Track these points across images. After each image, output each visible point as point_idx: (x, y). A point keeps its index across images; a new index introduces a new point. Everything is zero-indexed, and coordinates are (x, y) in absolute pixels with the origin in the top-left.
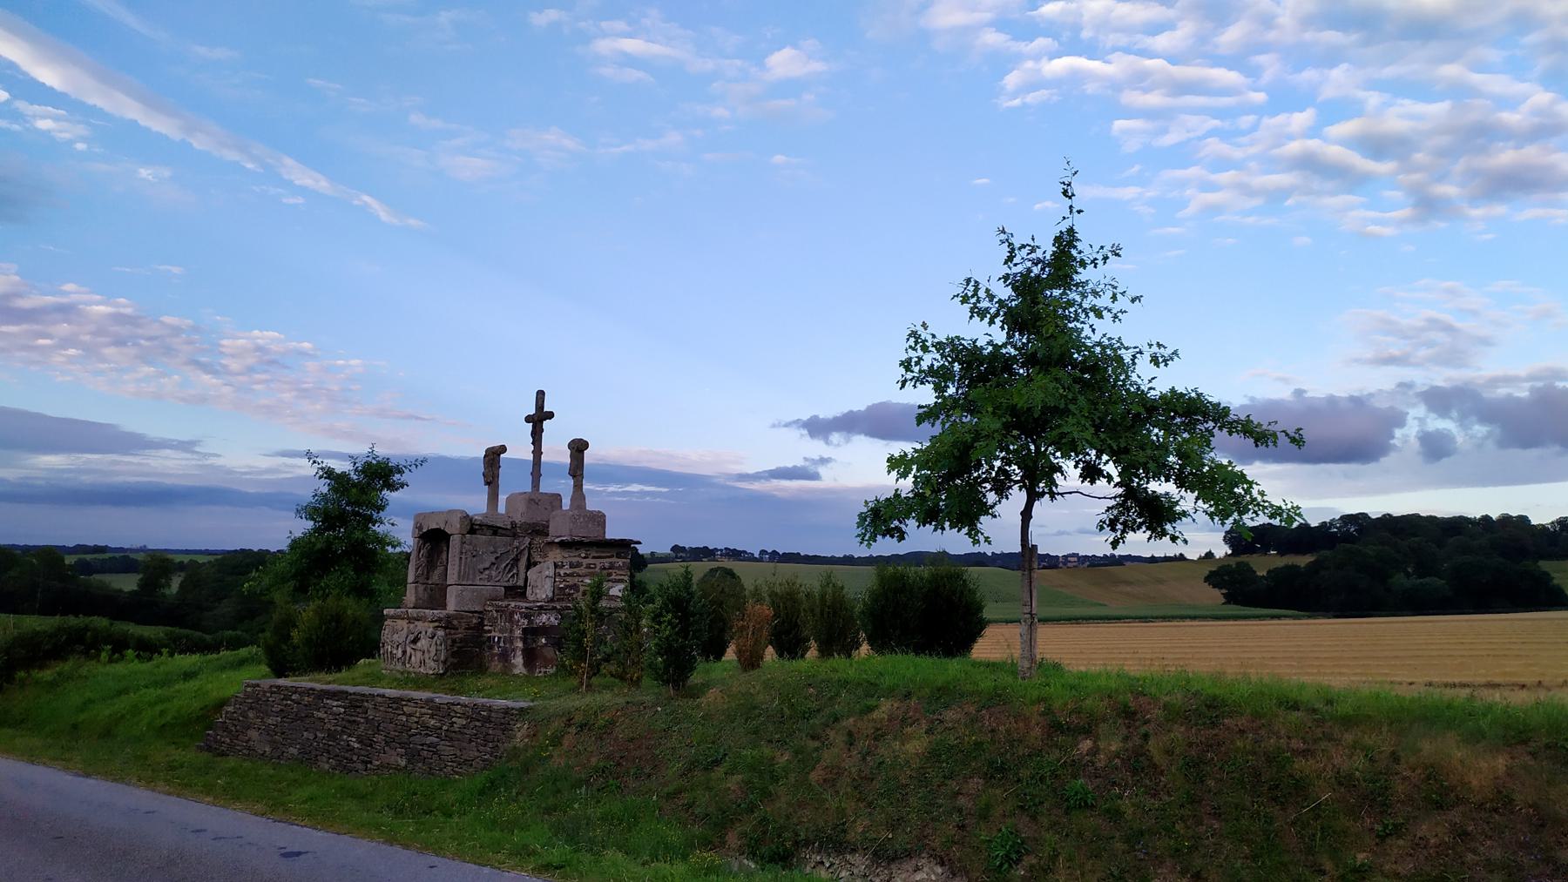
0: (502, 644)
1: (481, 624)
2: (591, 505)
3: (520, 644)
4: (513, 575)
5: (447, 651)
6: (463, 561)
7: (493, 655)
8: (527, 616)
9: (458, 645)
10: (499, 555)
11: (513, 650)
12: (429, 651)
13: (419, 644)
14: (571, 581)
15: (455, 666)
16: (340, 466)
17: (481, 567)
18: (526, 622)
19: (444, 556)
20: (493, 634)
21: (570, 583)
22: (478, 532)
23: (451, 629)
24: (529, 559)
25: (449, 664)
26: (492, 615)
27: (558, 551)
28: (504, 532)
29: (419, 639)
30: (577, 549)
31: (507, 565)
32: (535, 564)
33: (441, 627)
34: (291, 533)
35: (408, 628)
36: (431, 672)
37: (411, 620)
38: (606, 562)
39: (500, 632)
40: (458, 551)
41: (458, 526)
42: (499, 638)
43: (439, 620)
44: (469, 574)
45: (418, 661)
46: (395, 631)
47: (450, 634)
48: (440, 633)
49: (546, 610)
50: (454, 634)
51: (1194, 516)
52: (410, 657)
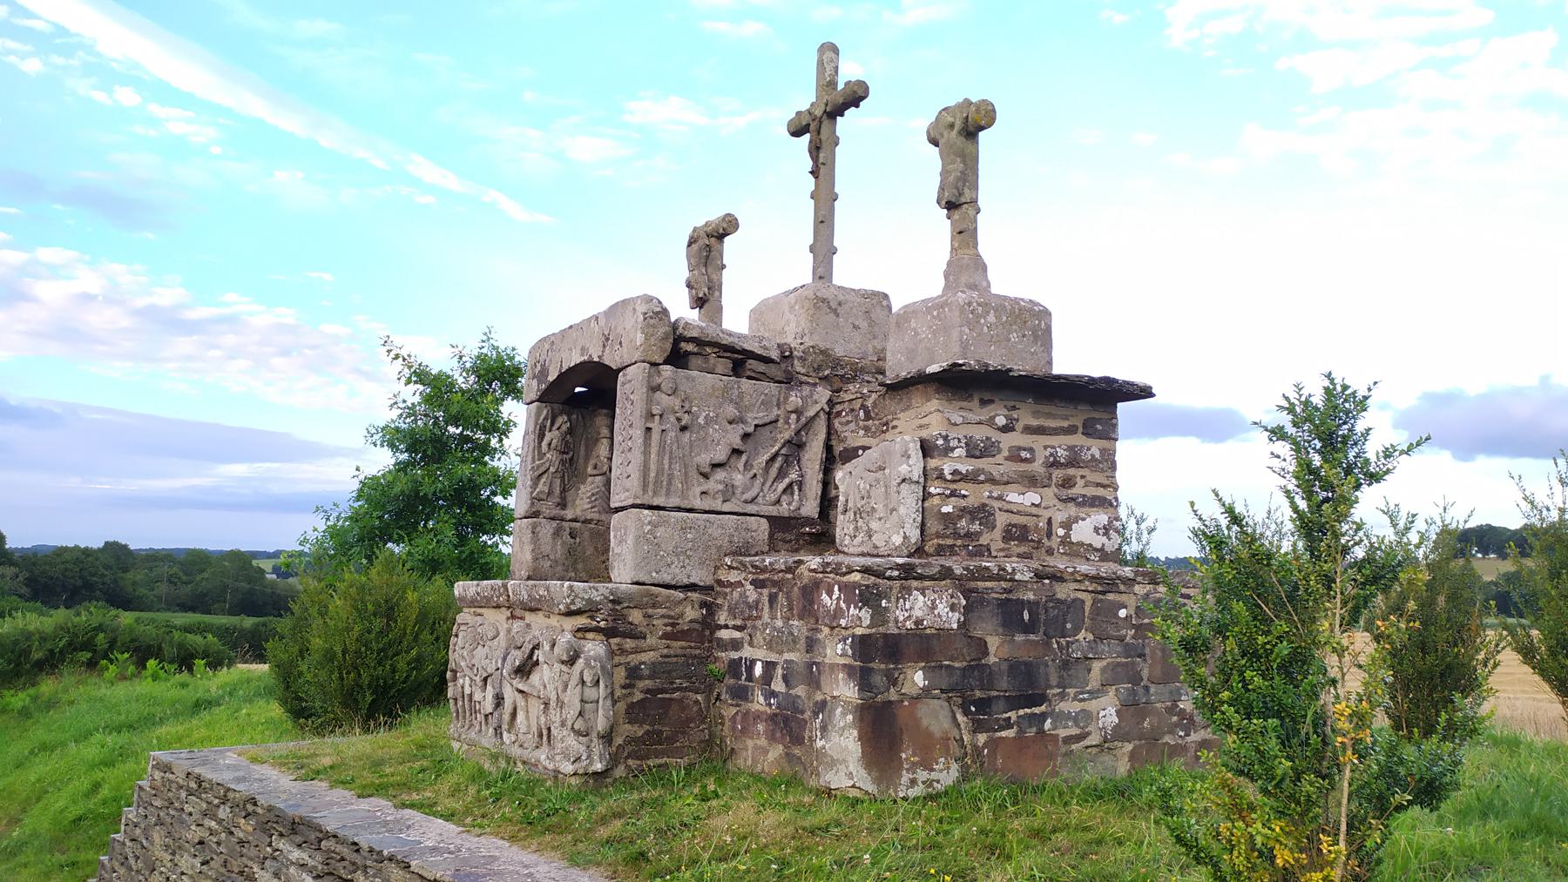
0: (778, 685)
1: (708, 624)
2: (1005, 281)
3: (847, 691)
4: (790, 485)
5: (614, 702)
6: (655, 436)
7: (750, 718)
8: (868, 598)
9: (648, 683)
10: (750, 429)
11: (821, 706)
12: (561, 704)
13: (535, 678)
14: (974, 495)
15: (641, 748)
16: (441, 361)
17: (704, 459)
18: (866, 615)
19: (603, 449)
20: (747, 652)
21: (972, 502)
22: (694, 361)
23: (625, 635)
24: (828, 448)
25: (619, 741)
26: (743, 595)
27: (934, 404)
28: (761, 367)
29: (537, 663)
30: (983, 403)
31: (773, 459)
32: (850, 454)
33: (597, 630)
34: (358, 469)
35: (509, 631)
36: (568, 768)
37: (518, 609)
38: (1060, 446)
39: (770, 648)
40: (639, 409)
41: (640, 338)
42: (769, 666)
43: (590, 610)
44: (671, 477)
45: (534, 729)
46: (479, 641)
47: (623, 651)
48: (594, 647)
49: (921, 578)
50: (636, 651)
51: (528, 647)
52: (514, 715)
